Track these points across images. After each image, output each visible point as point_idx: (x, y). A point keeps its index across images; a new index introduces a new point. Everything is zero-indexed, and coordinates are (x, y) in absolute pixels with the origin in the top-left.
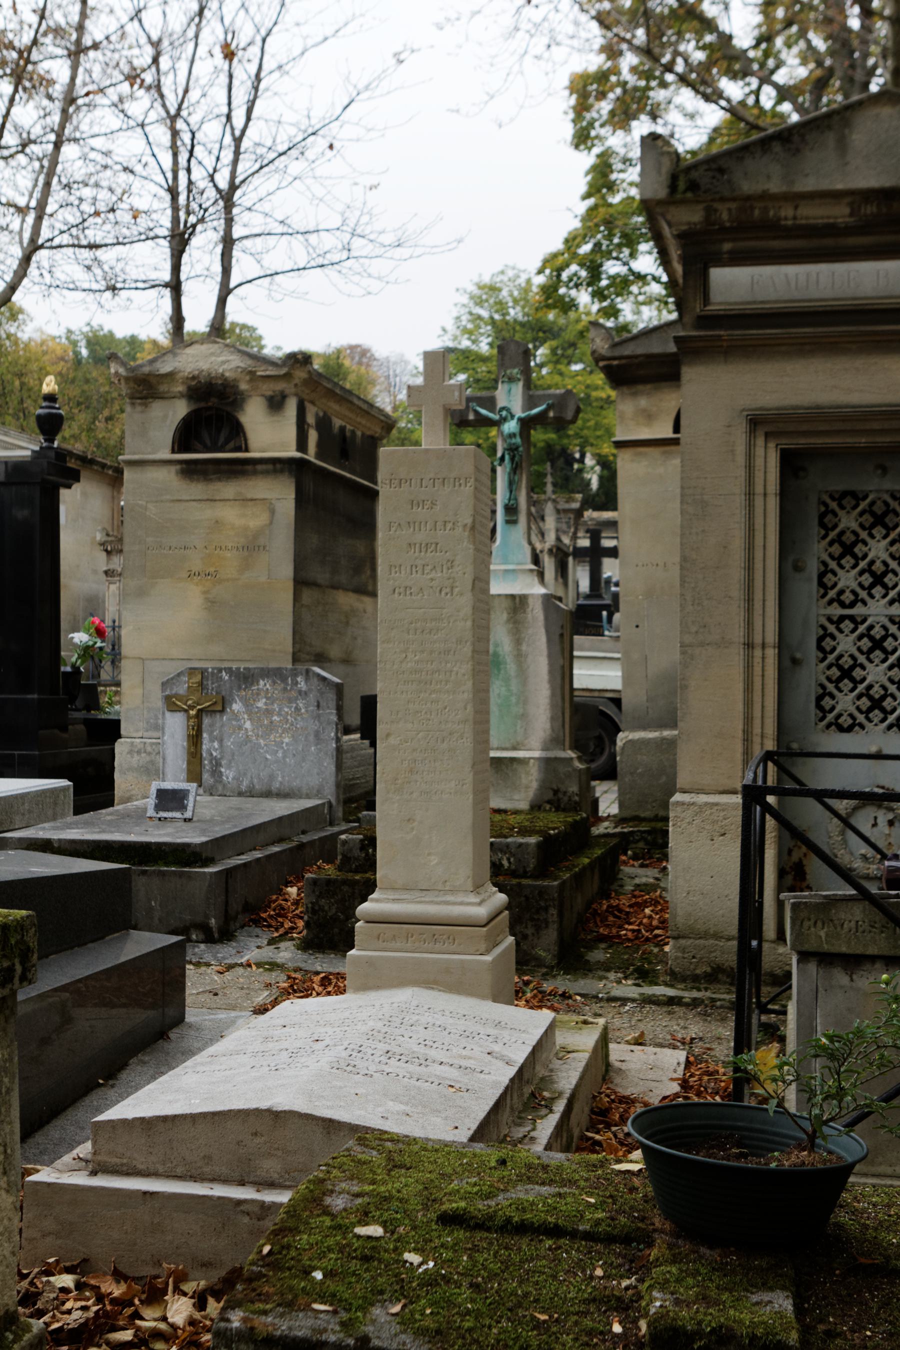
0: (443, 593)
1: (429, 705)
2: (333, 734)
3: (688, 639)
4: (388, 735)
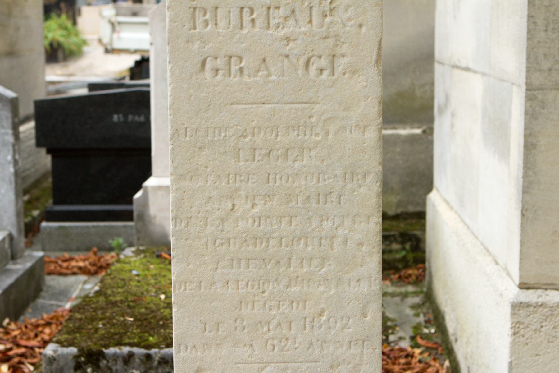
0: (313, 69)
1: (284, 308)
2: (10, 158)
3: (538, 79)
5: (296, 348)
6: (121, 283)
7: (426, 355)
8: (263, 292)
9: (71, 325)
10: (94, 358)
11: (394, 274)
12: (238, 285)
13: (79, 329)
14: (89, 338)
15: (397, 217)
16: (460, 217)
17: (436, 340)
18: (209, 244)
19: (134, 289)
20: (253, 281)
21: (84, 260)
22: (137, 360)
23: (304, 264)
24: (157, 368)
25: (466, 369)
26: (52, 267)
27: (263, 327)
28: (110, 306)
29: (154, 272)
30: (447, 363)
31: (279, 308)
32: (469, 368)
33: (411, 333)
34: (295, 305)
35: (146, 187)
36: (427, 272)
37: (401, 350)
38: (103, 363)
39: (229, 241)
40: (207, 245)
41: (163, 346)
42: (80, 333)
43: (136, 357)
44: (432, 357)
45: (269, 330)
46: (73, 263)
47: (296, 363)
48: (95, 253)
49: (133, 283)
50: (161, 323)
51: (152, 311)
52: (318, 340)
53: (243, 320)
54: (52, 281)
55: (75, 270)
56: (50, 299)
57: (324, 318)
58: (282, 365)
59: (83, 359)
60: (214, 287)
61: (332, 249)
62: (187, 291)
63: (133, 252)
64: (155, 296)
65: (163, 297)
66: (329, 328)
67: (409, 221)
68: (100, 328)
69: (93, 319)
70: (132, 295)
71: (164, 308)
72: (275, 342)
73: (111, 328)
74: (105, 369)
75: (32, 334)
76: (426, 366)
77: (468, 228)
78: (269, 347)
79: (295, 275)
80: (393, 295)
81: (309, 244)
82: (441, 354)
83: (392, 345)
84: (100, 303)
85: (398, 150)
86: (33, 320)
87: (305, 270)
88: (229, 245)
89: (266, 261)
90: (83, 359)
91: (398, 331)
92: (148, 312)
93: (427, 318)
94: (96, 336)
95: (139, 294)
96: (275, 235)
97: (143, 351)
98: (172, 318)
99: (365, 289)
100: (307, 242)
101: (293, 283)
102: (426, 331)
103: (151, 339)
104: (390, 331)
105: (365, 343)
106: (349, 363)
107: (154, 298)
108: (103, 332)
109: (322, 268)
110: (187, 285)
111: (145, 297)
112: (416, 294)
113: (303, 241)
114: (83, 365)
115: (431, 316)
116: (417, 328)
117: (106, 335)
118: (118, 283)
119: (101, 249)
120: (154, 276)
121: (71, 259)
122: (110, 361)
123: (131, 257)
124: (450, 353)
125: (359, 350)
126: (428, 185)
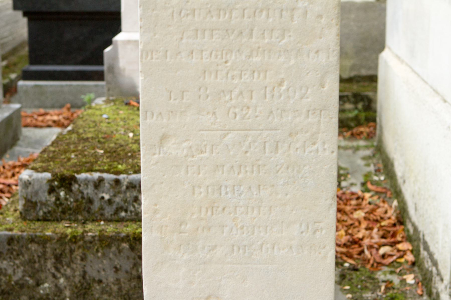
4: (164, 138)
5: (257, 117)
6: (92, 125)
7: (375, 198)
8: (226, 62)
9: (46, 156)
10: (67, 182)
11: (347, 131)
12: (202, 54)
13: (53, 159)
14: (62, 166)
15: (350, 80)
16: (410, 67)
17: (384, 186)
18: (175, 14)
19: (104, 129)
20: (217, 51)
21: (58, 115)
22: (107, 185)
23: (266, 35)
24: (125, 192)
25: (414, 206)
26: (29, 120)
27: (225, 96)
28: (82, 141)
29: (123, 116)
30: (395, 203)
31: (241, 78)
32: (416, 204)
33: (362, 180)
34: (256, 74)
35: (116, 41)
36: (378, 127)
37: (353, 194)
38: (75, 187)
39: (194, 12)
40: (173, 16)
41: (132, 172)
42: (54, 162)
43: (105, 181)
44: (381, 199)
45: (231, 99)
46: (48, 117)
47: (257, 130)
48: (69, 109)
49: (104, 125)
50: (129, 154)
51: (121, 146)
52: (278, 109)
53: (207, 89)
54: (26, 132)
55: (50, 123)
56: (27, 147)
57: (284, 88)
58: (243, 132)
59: (56, 183)
60: (179, 57)
61: (293, 21)
62: (154, 60)
63: (104, 101)
64: (124, 135)
65: (131, 135)
66: (289, 97)
67: (361, 84)
68: (73, 158)
69: (65, 152)
70: (102, 133)
71: (132, 143)
72: (237, 110)
73: (83, 158)
74: (77, 193)
75: (9, 174)
76: (375, 207)
77: (419, 75)
78: (231, 115)
79: (257, 45)
80: (345, 148)
81: (270, 15)
82: (390, 198)
83: (344, 190)
84: (73, 139)
85: (353, 16)
86: (11, 163)
87: (266, 41)
88: (194, 16)
89: (230, 32)
90: (56, 183)
91: (350, 179)
92: (117, 146)
93: (377, 168)
94: (69, 164)
95: (109, 132)
96: (237, 6)
97: (113, 177)
98: (139, 151)
99: (324, 61)
100: (268, 14)
101: (255, 53)
102: (376, 178)
103: (120, 166)
104: (342, 178)
105: (323, 112)
106: (307, 132)
107: (123, 136)
108: (76, 161)
109: (283, 39)
110: (154, 54)
111: (115, 135)
112: (367, 147)
113: (264, 13)
114: (56, 189)
115: (381, 166)
116: (367, 176)
117: (78, 163)
118: (89, 125)
119: (73, 106)
120: (124, 120)
121: (46, 114)
122: (82, 185)
123: (102, 105)
124: (398, 194)
125: (316, 120)
126: (380, 45)
